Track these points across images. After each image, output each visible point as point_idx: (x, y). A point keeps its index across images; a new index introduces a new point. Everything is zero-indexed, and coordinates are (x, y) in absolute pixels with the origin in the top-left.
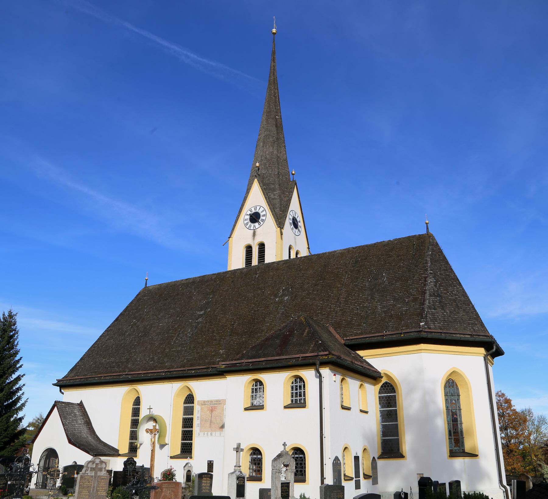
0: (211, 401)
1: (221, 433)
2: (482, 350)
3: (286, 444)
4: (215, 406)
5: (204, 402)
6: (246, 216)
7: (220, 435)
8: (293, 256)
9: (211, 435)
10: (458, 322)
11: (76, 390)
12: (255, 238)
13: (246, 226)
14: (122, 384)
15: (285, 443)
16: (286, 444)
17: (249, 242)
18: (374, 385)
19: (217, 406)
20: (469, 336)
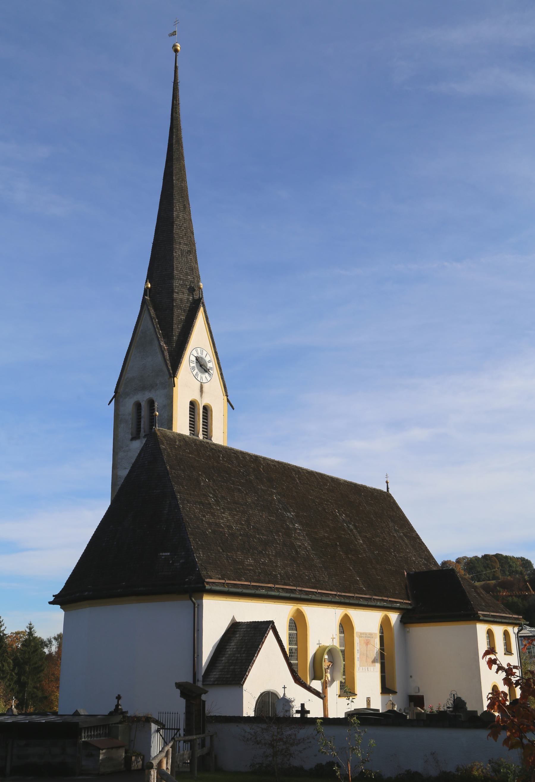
0: (366, 634)
1: (374, 668)
3: (116, 699)
4: (369, 639)
5: (361, 634)
7: (374, 670)
11: (225, 599)
12: (203, 396)
13: (196, 377)
14: (347, 606)
15: (119, 695)
16: (116, 699)
17: (196, 396)
19: (369, 639)
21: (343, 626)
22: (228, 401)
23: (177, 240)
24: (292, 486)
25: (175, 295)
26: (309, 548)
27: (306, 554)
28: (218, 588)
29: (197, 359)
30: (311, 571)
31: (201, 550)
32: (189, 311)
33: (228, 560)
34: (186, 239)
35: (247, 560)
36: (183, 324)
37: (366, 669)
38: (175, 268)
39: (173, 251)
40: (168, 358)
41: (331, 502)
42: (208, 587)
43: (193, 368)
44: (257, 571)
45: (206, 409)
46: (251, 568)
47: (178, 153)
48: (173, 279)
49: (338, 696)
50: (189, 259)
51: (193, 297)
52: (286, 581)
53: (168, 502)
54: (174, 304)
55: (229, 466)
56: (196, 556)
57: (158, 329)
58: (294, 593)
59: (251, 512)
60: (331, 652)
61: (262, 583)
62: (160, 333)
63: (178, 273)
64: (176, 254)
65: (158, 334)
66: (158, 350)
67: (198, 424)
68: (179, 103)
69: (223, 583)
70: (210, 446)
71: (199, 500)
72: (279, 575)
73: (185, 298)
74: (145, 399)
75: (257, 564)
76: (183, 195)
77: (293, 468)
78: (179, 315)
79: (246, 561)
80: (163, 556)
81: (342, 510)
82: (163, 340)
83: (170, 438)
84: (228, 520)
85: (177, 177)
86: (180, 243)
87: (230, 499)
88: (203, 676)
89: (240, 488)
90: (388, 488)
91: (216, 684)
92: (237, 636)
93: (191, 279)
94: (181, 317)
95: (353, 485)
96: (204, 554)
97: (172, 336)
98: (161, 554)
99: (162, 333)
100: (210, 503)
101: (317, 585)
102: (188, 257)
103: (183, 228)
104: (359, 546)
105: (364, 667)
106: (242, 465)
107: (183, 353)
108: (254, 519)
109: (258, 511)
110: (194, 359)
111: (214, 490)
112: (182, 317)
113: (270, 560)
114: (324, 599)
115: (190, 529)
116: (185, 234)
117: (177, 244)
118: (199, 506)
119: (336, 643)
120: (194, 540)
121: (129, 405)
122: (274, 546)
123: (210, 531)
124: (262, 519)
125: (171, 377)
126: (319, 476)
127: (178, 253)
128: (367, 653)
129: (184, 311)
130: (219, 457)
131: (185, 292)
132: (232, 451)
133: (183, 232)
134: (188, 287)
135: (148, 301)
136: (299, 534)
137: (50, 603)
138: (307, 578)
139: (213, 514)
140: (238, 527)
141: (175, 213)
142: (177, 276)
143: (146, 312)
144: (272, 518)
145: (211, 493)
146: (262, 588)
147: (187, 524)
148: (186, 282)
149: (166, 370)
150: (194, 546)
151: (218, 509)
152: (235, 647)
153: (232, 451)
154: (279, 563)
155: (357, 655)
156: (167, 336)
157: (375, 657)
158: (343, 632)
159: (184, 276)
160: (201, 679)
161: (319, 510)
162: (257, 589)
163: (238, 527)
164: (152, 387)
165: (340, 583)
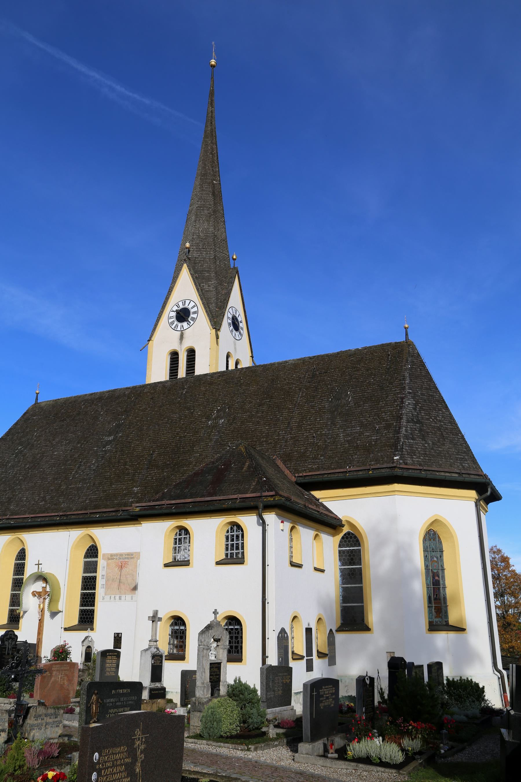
0: (121, 555)
2: (473, 494)
4: (126, 560)
5: (112, 555)
6: (171, 312)
7: (132, 599)
8: (232, 367)
13: (171, 326)
17: (175, 346)
18: (333, 535)
20: (456, 475)
37: (117, 598)
128: (121, 578)
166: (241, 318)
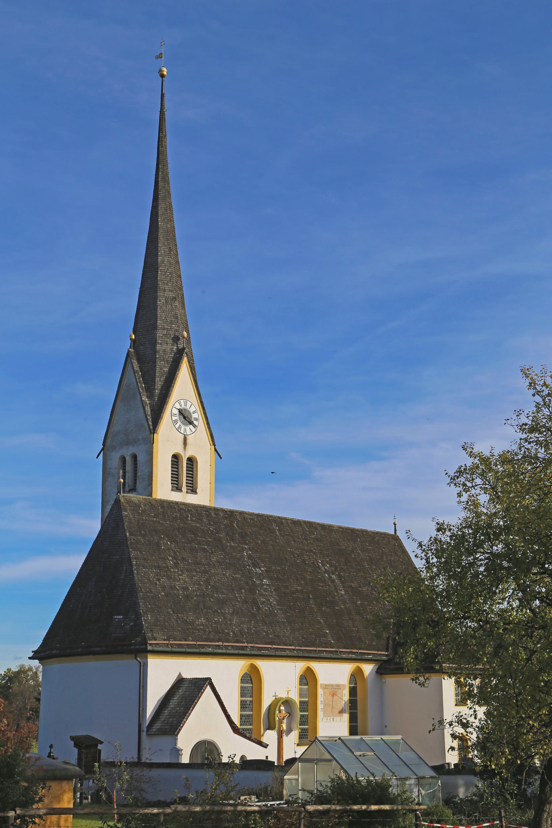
0: (332, 685)
1: (341, 719)
4: (336, 690)
5: (326, 685)
7: (341, 720)
9: (333, 720)
10: (460, 621)
13: (179, 430)
17: (179, 449)
21: (307, 678)
22: (216, 450)
23: (161, 288)
24: (268, 539)
25: (158, 347)
26: (275, 603)
27: (270, 609)
28: (161, 649)
29: (181, 412)
30: (272, 626)
31: (150, 613)
32: (172, 362)
33: (177, 621)
34: (171, 285)
35: (198, 620)
36: (166, 377)
37: (332, 719)
38: (158, 318)
39: (157, 299)
40: (149, 413)
41: (314, 553)
42: (149, 648)
43: (175, 422)
44: (207, 630)
45: (191, 461)
46: (202, 627)
47: (164, 191)
48: (157, 329)
49: (296, 744)
50: (174, 307)
51: (178, 347)
52: (238, 638)
53: (125, 568)
54: (157, 356)
55: (198, 525)
56: (144, 619)
57: (140, 383)
58: (244, 650)
59: (213, 571)
60: (287, 703)
61: (211, 641)
62: (142, 387)
63: (162, 322)
64: (160, 303)
65: (140, 388)
66: (140, 405)
67: (181, 477)
68: (165, 135)
69: (168, 644)
70: (178, 507)
71: (156, 564)
72: (231, 633)
73: (169, 349)
74: (129, 454)
75: (209, 624)
76: (168, 238)
77: (275, 519)
78: (162, 367)
79: (197, 621)
80: (117, 618)
81: (327, 560)
82: (145, 394)
83: (135, 503)
84: (185, 582)
85: (163, 218)
86: (165, 290)
87: (191, 560)
88: (147, 727)
89: (206, 547)
90: (395, 530)
91: (154, 734)
92: (180, 691)
93: (175, 328)
94: (163, 369)
95: (349, 531)
96: (152, 617)
97: (154, 389)
98: (115, 617)
99: (145, 387)
100: (168, 566)
101: (275, 641)
102: (173, 304)
103: (168, 273)
104: (339, 597)
105: (329, 718)
106: (213, 522)
107: (164, 407)
108: (215, 578)
109: (222, 569)
110: (177, 412)
111: (175, 553)
112: (165, 369)
113: (225, 618)
114: (278, 653)
115: (141, 594)
116: (170, 279)
117: (161, 292)
118: (156, 570)
119: (295, 697)
120: (143, 604)
121: (115, 461)
122: (232, 604)
123: (163, 594)
124: (224, 578)
125: (151, 433)
126: (306, 525)
127: (162, 301)
128: (333, 704)
129: (167, 362)
130: (188, 516)
131: (168, 342)
132: (204, 509)
133: (168, 278)
134: (172, 336)
135: (131, 354)
136: (266, 590)
137: (30, 658)
138: (264, 634)
139: (169, 578)
140: (195, 588)
141: (159, 258)
142: (160, 326)
143: (130, 365)
144: (236, 576)
145: (171, 556)
146: (209, 646)
147: (140, 589)
148: (171, 332)
149: (147, 426)
150: (143, 610)
151: (175, 571)
152: (177, 701)
153: (204, 509)
154: (234, 621)
155: (320, 706)
156: (150, 390)
157: (343, 708)
158: (307, 683)
159: (169, 325)
160: (145, 729)
161: (297, 562)
162: (203, 648)
163: (195, 588)
164: (135, 442)
165: (304, 637)
166: (194, 409)
